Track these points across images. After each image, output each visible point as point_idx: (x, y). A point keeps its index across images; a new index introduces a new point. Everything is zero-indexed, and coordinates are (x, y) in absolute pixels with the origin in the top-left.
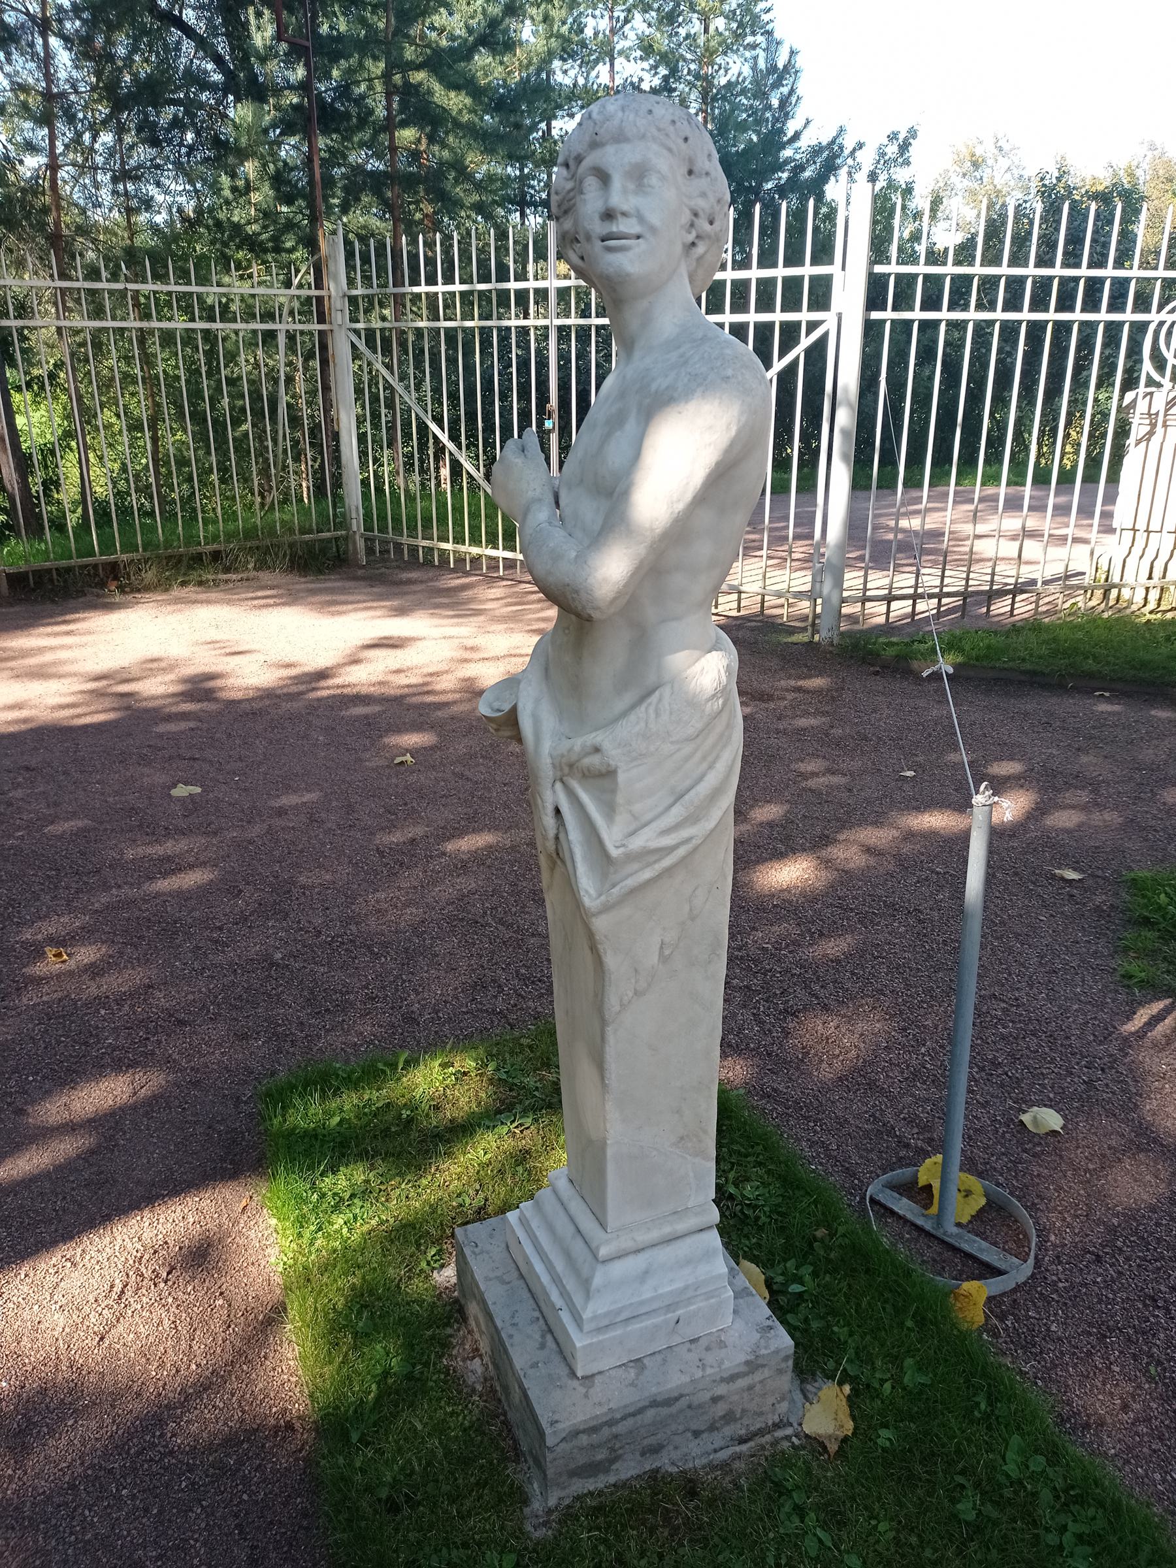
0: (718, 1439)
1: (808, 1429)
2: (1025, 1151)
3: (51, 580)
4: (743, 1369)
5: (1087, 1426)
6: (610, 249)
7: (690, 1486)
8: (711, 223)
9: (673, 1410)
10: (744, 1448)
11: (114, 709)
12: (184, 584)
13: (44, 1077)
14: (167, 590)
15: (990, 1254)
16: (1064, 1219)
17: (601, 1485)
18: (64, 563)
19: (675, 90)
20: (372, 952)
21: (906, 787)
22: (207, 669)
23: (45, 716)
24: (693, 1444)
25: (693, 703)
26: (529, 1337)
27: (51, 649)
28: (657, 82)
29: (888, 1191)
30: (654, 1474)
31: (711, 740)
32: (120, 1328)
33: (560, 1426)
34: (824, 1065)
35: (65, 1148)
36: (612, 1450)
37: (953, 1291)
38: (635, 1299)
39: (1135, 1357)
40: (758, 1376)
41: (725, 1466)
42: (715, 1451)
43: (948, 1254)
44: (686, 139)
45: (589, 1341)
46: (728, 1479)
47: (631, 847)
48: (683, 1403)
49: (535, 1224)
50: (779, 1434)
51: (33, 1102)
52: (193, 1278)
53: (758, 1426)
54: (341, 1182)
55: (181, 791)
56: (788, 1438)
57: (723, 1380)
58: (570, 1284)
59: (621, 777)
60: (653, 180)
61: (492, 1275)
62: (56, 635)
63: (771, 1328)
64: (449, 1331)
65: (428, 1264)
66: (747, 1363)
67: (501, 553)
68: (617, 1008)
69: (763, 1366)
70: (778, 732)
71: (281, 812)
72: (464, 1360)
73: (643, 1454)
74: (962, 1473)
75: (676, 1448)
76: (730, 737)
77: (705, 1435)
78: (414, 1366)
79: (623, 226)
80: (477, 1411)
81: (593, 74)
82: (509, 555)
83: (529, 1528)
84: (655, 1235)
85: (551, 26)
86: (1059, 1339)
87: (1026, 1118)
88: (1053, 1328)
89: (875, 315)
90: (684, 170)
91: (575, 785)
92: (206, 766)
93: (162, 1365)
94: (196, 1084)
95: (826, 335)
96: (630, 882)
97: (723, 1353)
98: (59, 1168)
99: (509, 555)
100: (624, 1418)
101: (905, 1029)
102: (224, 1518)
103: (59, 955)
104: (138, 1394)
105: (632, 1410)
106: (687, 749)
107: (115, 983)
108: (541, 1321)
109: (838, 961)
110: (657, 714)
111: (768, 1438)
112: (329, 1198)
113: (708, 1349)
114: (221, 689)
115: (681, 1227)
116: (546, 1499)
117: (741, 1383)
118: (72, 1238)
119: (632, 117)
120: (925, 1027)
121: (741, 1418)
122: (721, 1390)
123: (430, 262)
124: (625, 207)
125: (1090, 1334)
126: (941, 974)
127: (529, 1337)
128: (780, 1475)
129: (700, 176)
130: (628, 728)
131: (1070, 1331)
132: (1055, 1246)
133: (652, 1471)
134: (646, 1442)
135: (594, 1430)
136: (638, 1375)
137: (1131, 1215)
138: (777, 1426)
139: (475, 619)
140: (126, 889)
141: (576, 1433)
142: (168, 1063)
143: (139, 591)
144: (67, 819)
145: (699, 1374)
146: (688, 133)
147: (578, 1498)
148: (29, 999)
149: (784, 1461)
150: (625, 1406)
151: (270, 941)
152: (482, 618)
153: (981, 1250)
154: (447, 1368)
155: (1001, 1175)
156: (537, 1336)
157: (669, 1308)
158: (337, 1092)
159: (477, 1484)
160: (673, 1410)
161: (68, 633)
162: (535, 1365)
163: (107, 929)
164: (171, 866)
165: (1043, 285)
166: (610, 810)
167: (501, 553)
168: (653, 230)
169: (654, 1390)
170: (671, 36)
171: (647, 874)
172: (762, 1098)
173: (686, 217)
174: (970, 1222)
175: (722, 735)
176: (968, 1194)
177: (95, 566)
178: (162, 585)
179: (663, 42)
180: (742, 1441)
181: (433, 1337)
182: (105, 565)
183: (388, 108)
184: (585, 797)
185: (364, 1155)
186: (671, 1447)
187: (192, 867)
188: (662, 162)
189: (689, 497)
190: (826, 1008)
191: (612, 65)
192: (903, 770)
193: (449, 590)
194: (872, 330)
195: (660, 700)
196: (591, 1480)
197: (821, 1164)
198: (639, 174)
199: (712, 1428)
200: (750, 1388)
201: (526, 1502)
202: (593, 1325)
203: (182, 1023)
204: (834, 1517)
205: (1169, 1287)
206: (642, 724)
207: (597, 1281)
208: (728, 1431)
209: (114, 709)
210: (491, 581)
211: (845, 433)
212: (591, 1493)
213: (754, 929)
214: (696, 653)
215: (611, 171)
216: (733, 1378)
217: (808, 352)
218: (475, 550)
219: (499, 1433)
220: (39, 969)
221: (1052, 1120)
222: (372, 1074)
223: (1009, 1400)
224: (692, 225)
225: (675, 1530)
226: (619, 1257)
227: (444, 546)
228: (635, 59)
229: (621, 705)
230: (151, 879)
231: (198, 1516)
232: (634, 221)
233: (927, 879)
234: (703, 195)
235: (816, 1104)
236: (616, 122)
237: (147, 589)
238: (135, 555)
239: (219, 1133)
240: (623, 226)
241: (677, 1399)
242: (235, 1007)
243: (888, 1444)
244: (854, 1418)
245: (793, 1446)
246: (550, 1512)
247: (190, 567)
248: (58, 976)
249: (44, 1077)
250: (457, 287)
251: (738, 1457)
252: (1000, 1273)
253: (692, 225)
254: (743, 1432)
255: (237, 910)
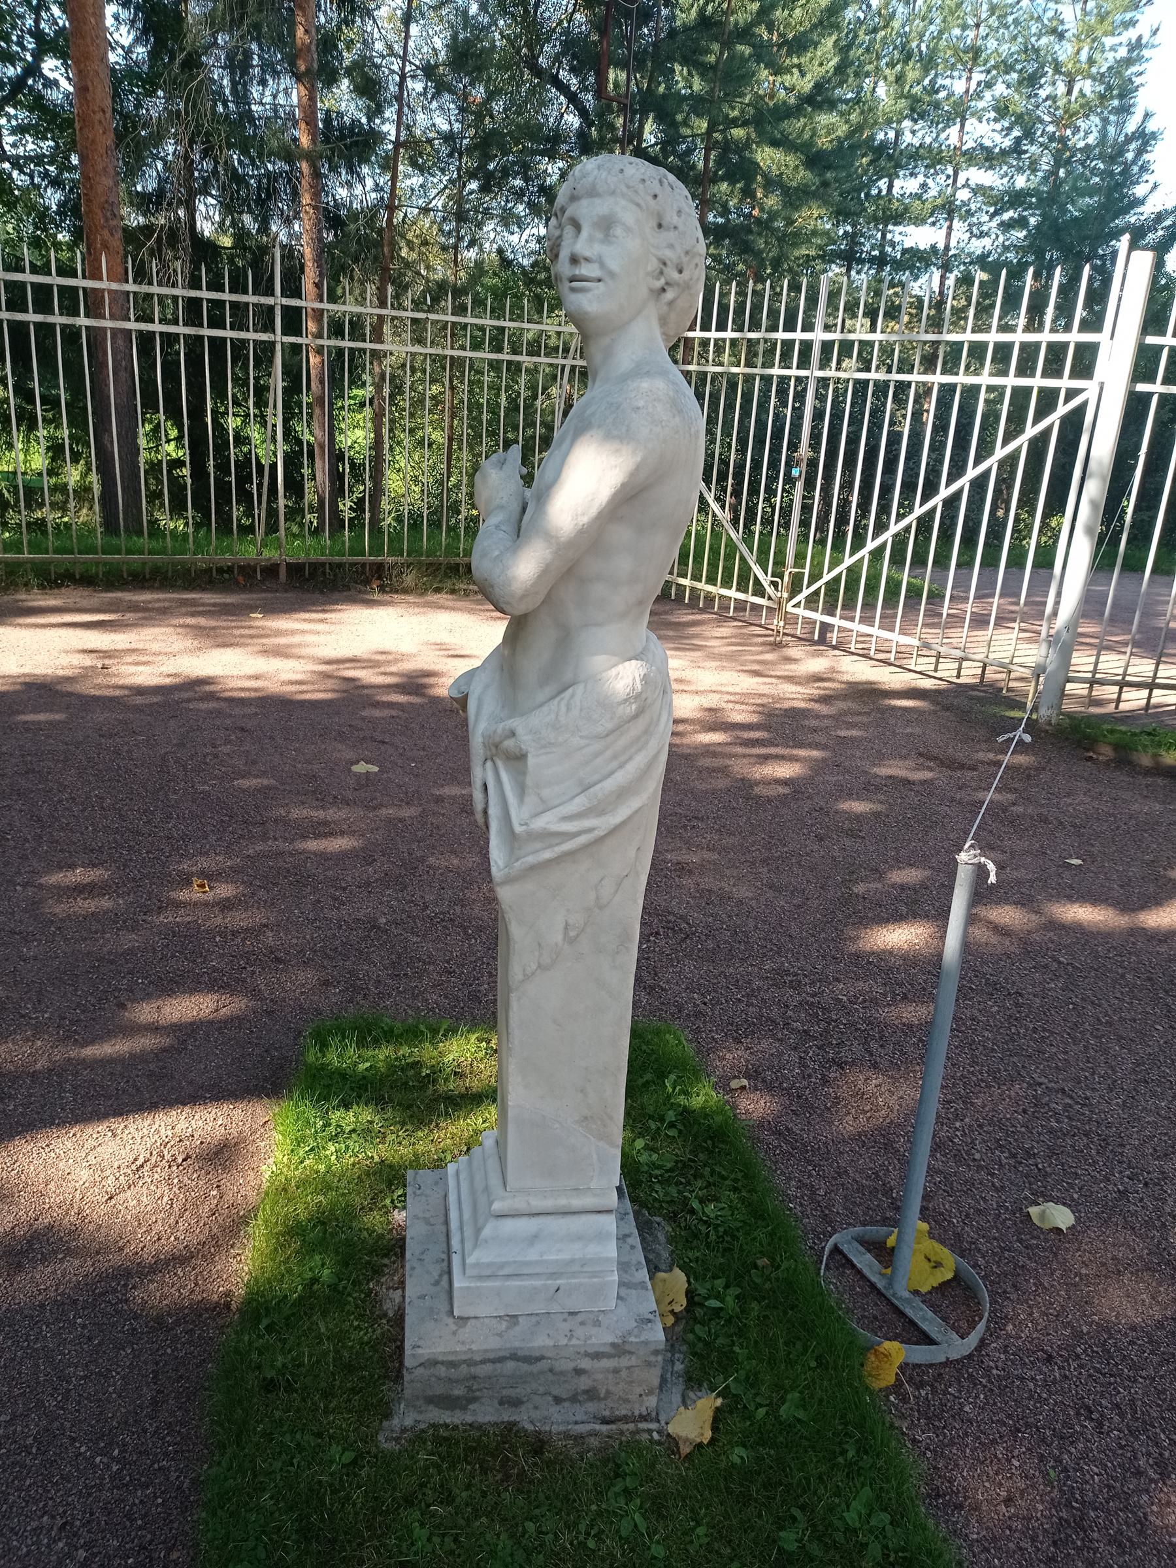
0: (579, 1412)
1: (671, 1429)
2: (1020, 1241)
3: (324, 573)
4: (608, 1349)
5: (960, 1507)
6: (573, 290)
7: (538, 1444)
8: (680, 272)
9: (535, 1368)
10: (604, 1428)
11: (334, 691)
12: (438, 590)
13: (151, 982)
14: (422, 594)
15: (928, 1321)
16: (1031, 1314)
17: (457, 1421)
18: (337, 559)
19: (1026, 152)
20: (466, 933)
21: (1067, 874)
22: (426, 667)
23: (272, 687)
24: (554, 1409)
25: (606, 704)
26: (428, 1272)
27: (303, 632)
28: (1007, 143)
29: (856, 1244)
30: (510, 1426)
31: (623, 742)
32: (129, 1193)
33: (420, 1351)
34: (849, 1118)
35: (146, 1042)
36: (470, 1389)
37: (870, 1348)
38: (519, 1258)
39: (1041, 1458)
40: (625, 1362)
41: (579, 1439)
42: (576, 1423)
43: (892, 1316)
44: (655, 196)
45: (466, 1284)
46: (576, 1449)
47: (532, 826)
48: (544, 1365)
49: (462, 1176)
50: (643, 1425)
51: (135, 1000)
52: (201, 1168)
53: (624, 1412)
54: (347, 1118)
55: (361, 768)
56: (650, 1431)
57: (587, 1354)
58: (468, 1232)
59: (531, 761)
60: (618, 231)
61: (421, 1215)
62: (310, 621)
63: (650, 1321)
64: (386, 1261)
65: (392, 1202)
66: (613, 1345)
67: (732, 593)
68: (521, 977)
69: (631, 1353)
70: (953, 800)
71: (439, 800)
72: (388, 1289)
73: (501, 1403)
74: (802, 1508)
75: (536, 1408)
76: (647, 743)
77: (567, 1404)
78: (340, 1280)
79: (584, 270)
80: (379, 1331)
81: (943, 136)
82: (741, 596)
83: (381, 1438)
84: (548, 1204)
85: (902, 86)
86: (970, 1421)
87: (1033, 1211)
88: (967, 1409)
89: (1141, 387)
90: (655, 225)
91: (500, 764)
92: (391, 750)
93: (149, 1231)
94: (269, 1013)
95: (1084, 405)
96: (531, 859)
97: (594, 1330)
98: (132, 1056)
99: (741, 596)
100: (483, 1362)
101: (949, 1102)
102: (146, 1363)
103: (202, 886)
104: (121, 1249)
105: (492, 1356)
106: (597, 746)
107: (239, 919)
108: (445, 1264)
109: (910, 1026)
110: (568, 709)
111: (631, 1426)
112: (332, 1128)
113: (582, 1323)
114: (432, 686)
115: (577, 1202)
116: (406, 1417)
117: (606, 1363)
118: (121, 1115)
119: (604, 174)
120: (972, 1104)
121: (605, 1398)
122: (585, 1364)
123: (723, 309)
124: (587, 254)
125: (1004, 1424)
126: (1015, 1059)
127: (428, 1272)
128: (626, 1463)
129: (668, 229)
130: (537, 719)
131: (986, 1416)
132: (1009, 1336)
133: (509, 1423)
134: (504, 1392)
135: (452, 1364)
136: (508, 1328)
137: (1106, 1328)
138: (644, 1418)
139: (692, 654)
140: (280, 843)
141: (434, 1363)
142: (255, 993)
143: (397, 592)
144: (257, 777)
145: (564, 1341)
146: (658, 192)
147: (433, 1426)
148: (167, 918)
149: (632, 1446)
150: (486, 1351)
151: (382, 908)
152: (699, 654)
153: (924, 1319)
154: (370, 1291)
155: (983, 1257)
156: (436, 1275)
157: (553, 1275)
158: (376, 1042)
159: (353, 1389)
160: (535, 1368)
161: (321, 621)
162: (422, 1297)
163: (251, 872)
164: (324, 830)
165: (1029, 351)
166: (522, 790)
167: (732, 593)
168: (612, 274)
169: (517, 1344)
170: (1029, 97)
171: (547, 855)
172: (774, 1133)
173: (653, 265)
174: (930, 1292)
175: (638, 739)
176: (938, 1265)
177: (364, 565)
178: (420, 590)
179: (1020, 104)
180: (605, 1421)
181: (369, 1263)
182: (372, 564)
183: (706, 159)
184: (505, 777)
185: (380, 1102)
186: (530, 1406)
187: (342, 833)
188: (627, 215)
189: (593, 511)
190: (875, 1066)
191: (962, 126)
192: (1071, 857)
193: (679, 624)
194: (1135, 406)
195: (572, 696)
196: (448, 1413)
197: (801, 1205)
198: (606, 225)
199: (574, 1399)
200: (616, 1371)
201: (388, 1416)
202: (475, 1272)
203: (278, 960)
204: (657, 1508)
205: (1112, 1403)
206: (553, 716)
207: (487, 1232)
208: (591, 1407)
209: (334, 691)
210: (722, 618)
211: (1094, 504)
212: (446, 1425)
213: (838, 980)
214: (614, 659)
215: (582, 222)
216: (597, 1356)
217: (1064, 420)
218: (710, 588)
219: (388, 1350)
220: (182, 895)
221: (1061, 1217)
222: (412, 1035)
223: (878, 1455)
224: (661, 273)
225: (507, 1477)
226: (513, 1216)
227: (682, 581)
228: (988, 120)
229: (541, 696)
230: (304, 837)
231: (127, 1355)
232: (596, 266)
233: (1046, 966)
234: (671, 246)
235: (823, 1150)
236: (590, 179)
237: (405, 591)
238: (400, 560)
239: (272, 1058)
240: (584, 270)
241: (539, 1359)
242: (329, 957)
243: (739, 1461)
244: (714, 1428)
245: (651, 1440)
246: (404, 1430)
247: (446, 575)
248: (195, 904)
249: (151, 982)
250: (729, 334)
251: (595, 1434)
252: (932, 1342)
253: (661, 273)
254: (607, 1413)
255: (365, 876)
